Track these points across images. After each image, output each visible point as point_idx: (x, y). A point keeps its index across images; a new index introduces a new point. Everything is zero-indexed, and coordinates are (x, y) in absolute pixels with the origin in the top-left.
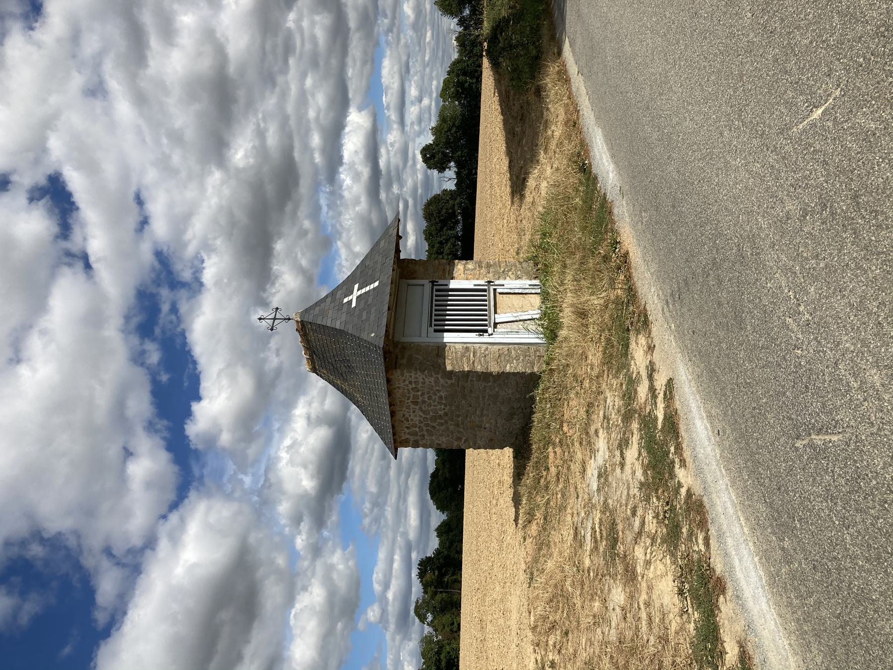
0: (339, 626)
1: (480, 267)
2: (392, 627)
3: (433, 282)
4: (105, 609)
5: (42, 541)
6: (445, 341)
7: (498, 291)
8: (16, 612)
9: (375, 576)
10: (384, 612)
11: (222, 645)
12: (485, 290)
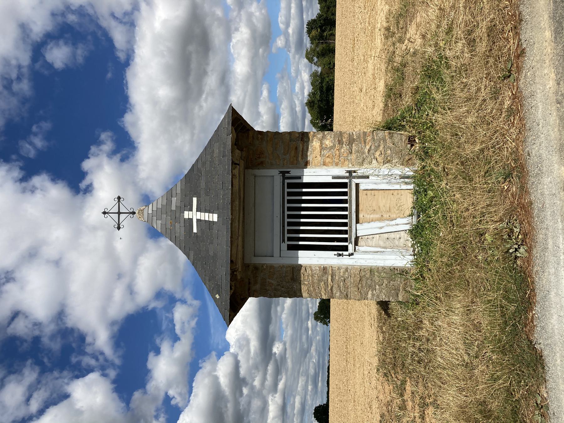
0: (261, 51)
1: (340, 142)
2: (293, 50)
3: (283, 173)
4: (122, 51)
5: (73, 12)
6: (300, 262)
7: (362, 187)
8: (74, 55)
9: (280, 18)
10: (287, 41)
11: (193, 65)
12: (344, 185)
